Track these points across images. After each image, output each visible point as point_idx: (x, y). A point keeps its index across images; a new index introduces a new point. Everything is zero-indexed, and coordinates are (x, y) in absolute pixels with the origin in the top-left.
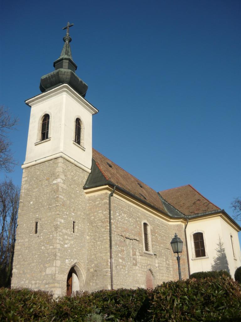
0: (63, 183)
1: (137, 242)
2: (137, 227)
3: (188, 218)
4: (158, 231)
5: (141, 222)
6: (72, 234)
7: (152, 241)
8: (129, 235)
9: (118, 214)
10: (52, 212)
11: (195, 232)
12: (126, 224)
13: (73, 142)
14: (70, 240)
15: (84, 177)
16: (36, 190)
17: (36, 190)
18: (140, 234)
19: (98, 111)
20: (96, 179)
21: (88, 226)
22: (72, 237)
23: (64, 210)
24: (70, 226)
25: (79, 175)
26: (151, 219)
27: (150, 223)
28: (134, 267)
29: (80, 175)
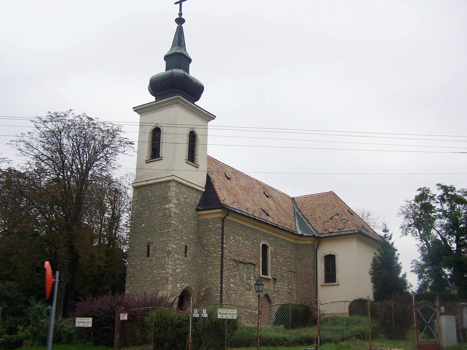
2: (254, 249)
4: (280, 253)
5: (259, 244)
10: (164, 238)
11: (327, 254)
14: (181, 265)
16: (148, 212)
17: (148, 212)
18: (257, 257)
21: (200, 249)
27: (270, 244)
28: (247, 292)
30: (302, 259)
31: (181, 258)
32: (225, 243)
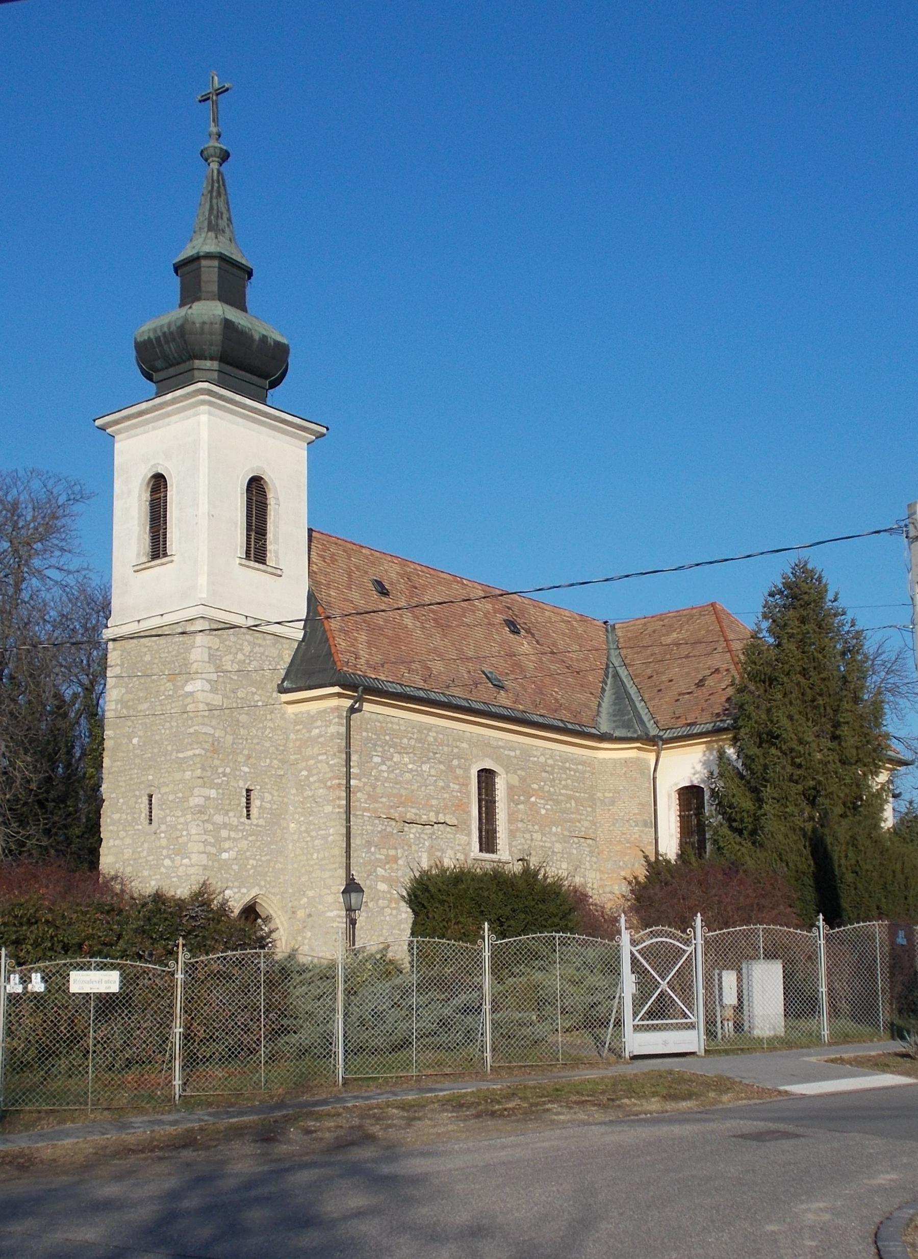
0: (211, 691)
1: (448, 829)
3: (661, 738)
5: (467, 770)
6: (243, 823)
7: (510, 821)
8: (416, 814)
9: (377, 760)
12: (408, 782)
13: (238, 561)
15: (280, 657)
18: (461, 807)
19: (328, 429)
20: (313, 665)
22: (243, 831)
23: (216, 762)
24: (237, 802)
25: (262, 654)
26: (512, 754)
29: (266, 654)
30: (613, 802)
31: (235, 822)
32: (357, 774)
